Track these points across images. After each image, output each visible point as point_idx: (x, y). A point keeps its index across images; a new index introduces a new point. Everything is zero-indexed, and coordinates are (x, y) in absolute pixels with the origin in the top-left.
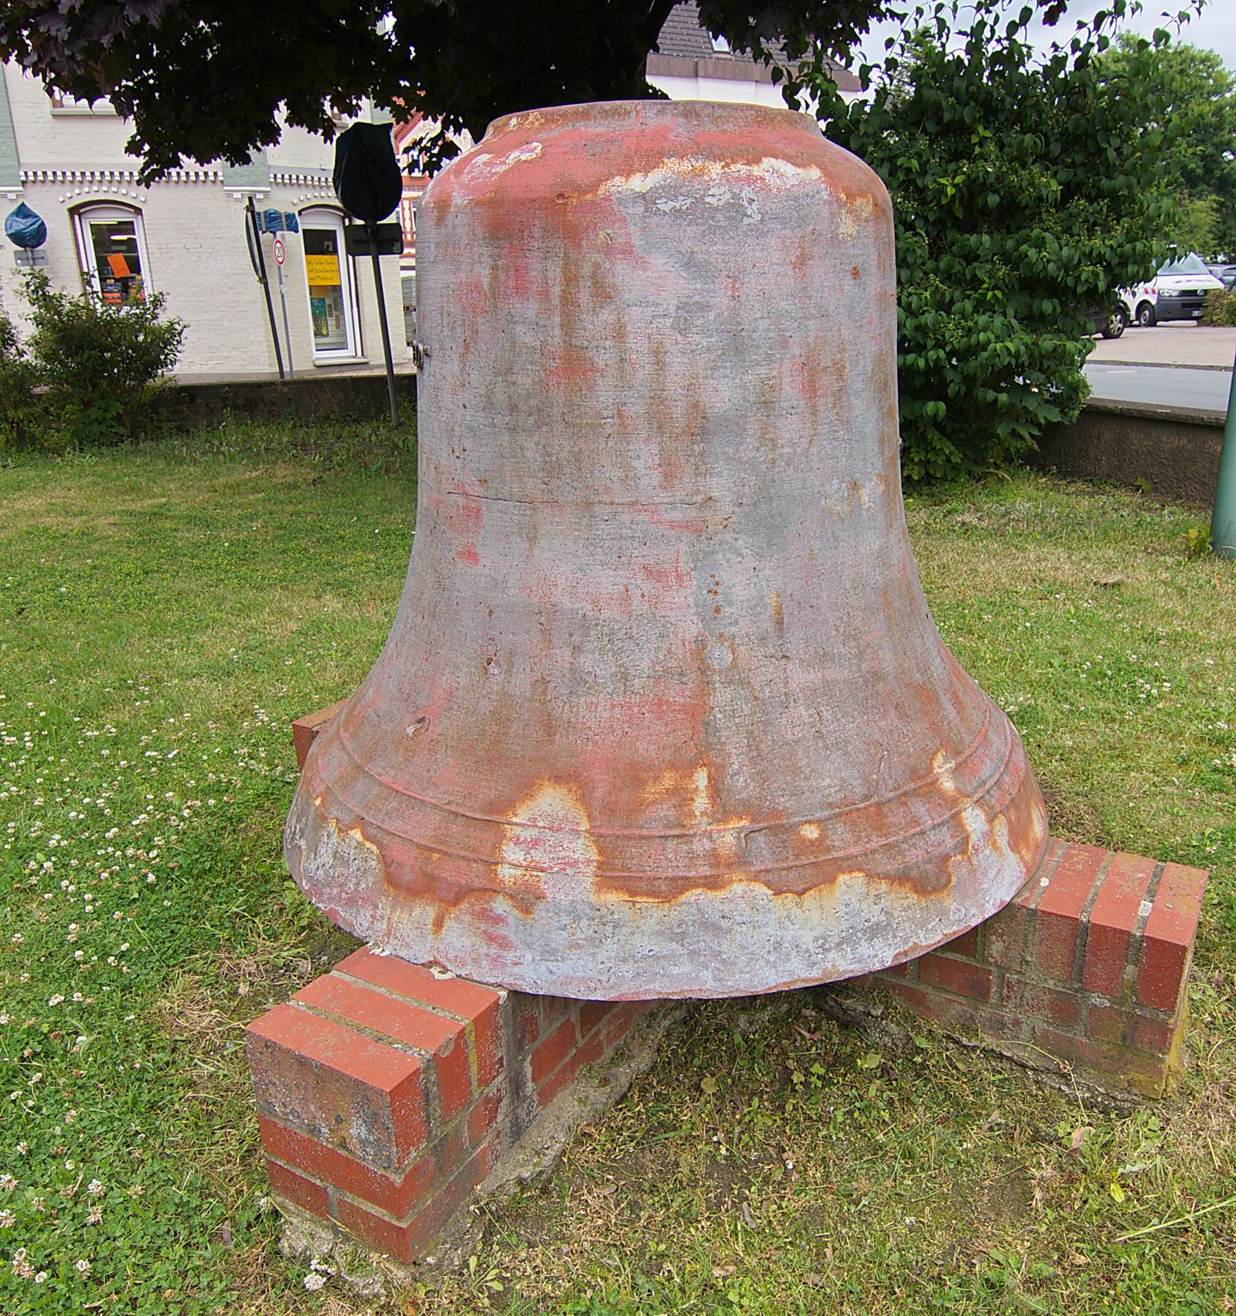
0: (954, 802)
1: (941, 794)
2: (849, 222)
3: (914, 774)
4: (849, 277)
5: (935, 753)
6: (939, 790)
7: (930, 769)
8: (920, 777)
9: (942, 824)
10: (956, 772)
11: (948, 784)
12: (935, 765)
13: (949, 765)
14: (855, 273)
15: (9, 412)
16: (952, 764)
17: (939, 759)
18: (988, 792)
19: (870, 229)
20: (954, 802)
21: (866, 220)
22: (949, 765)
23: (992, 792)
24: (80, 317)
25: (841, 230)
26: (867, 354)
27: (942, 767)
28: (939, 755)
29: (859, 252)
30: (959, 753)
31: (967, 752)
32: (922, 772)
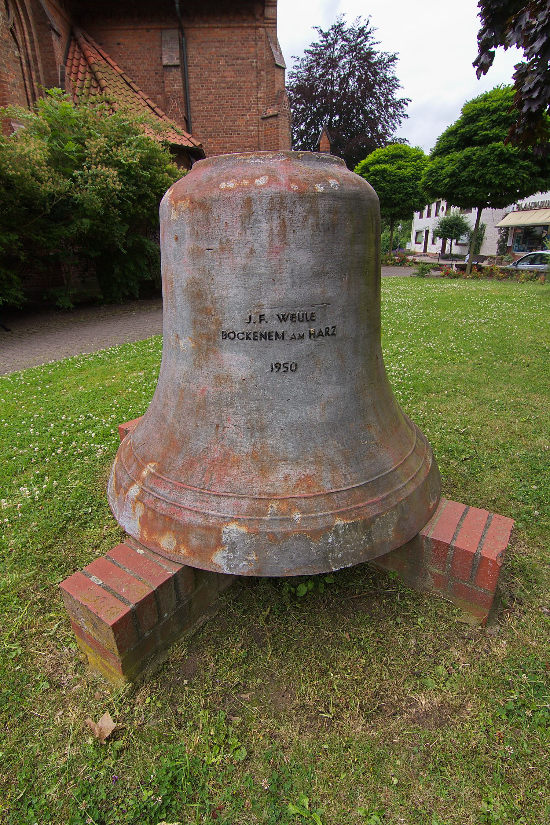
0: (139, 478)
1: (141, 472)
2: (175, 214)
3: (144, 458)
4: (174, 239)
5: (154, 461)
6: (141, 470)
7: (147, 463)
8: (144, 461)
9: (130, 477)
10: (151, 474)
11: (145, 473)
12: (150, 464)
13: (152, 469)
14: (176, 239)
15: (472, 190)
16: (153, 471)
17: (152, 465)
18: (150, 494)
19: (187, 216)
20: (139, 478)
21: (184, 211)
22: (152, 469)
23: (151, 496)
24: (84, 233)
25: (172, 218)
26: (183, 277)
27: (150, 468)
28: (154, 464)
29: (179, 228)
30: (160, 473)
31: (163, 477)
32: (146, 460)
